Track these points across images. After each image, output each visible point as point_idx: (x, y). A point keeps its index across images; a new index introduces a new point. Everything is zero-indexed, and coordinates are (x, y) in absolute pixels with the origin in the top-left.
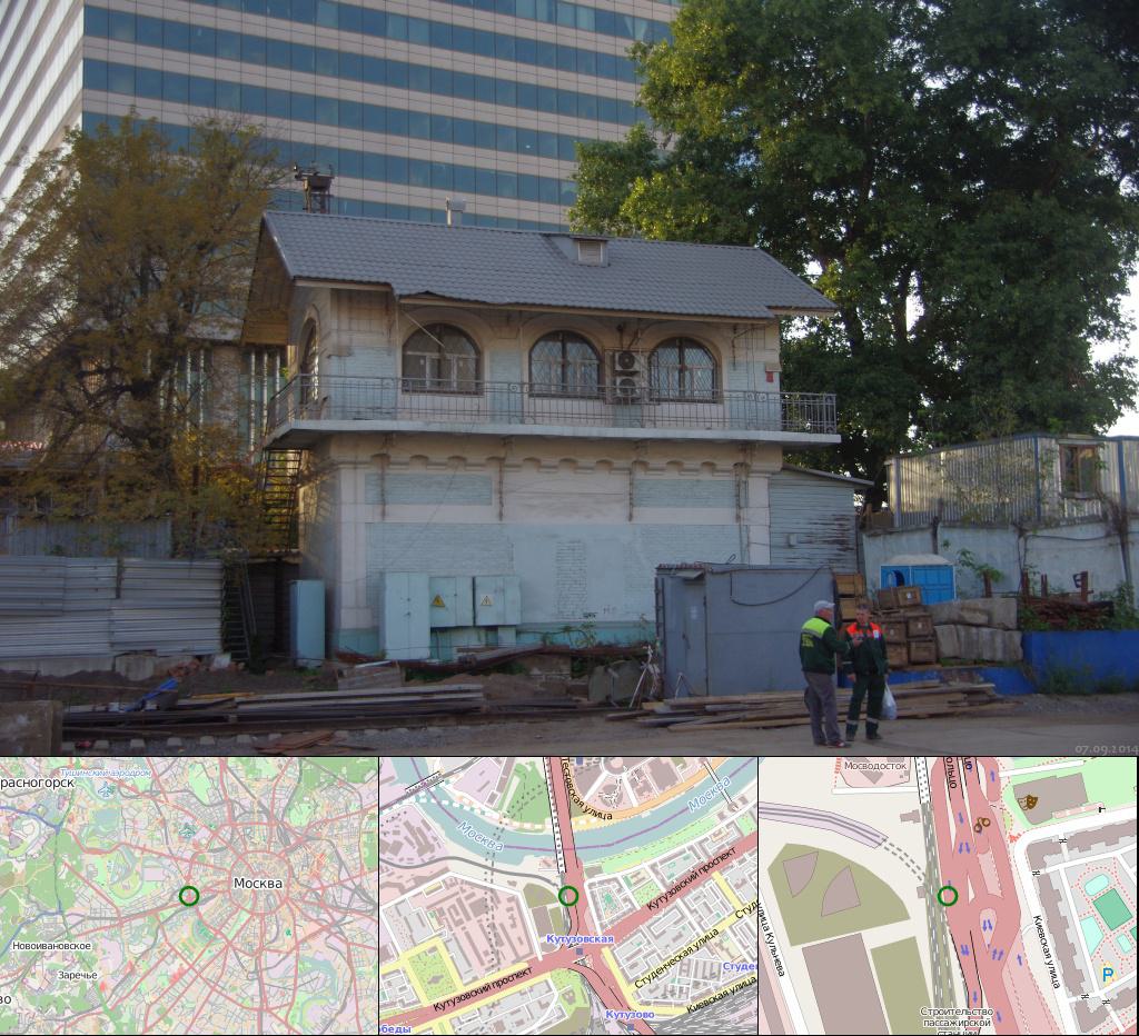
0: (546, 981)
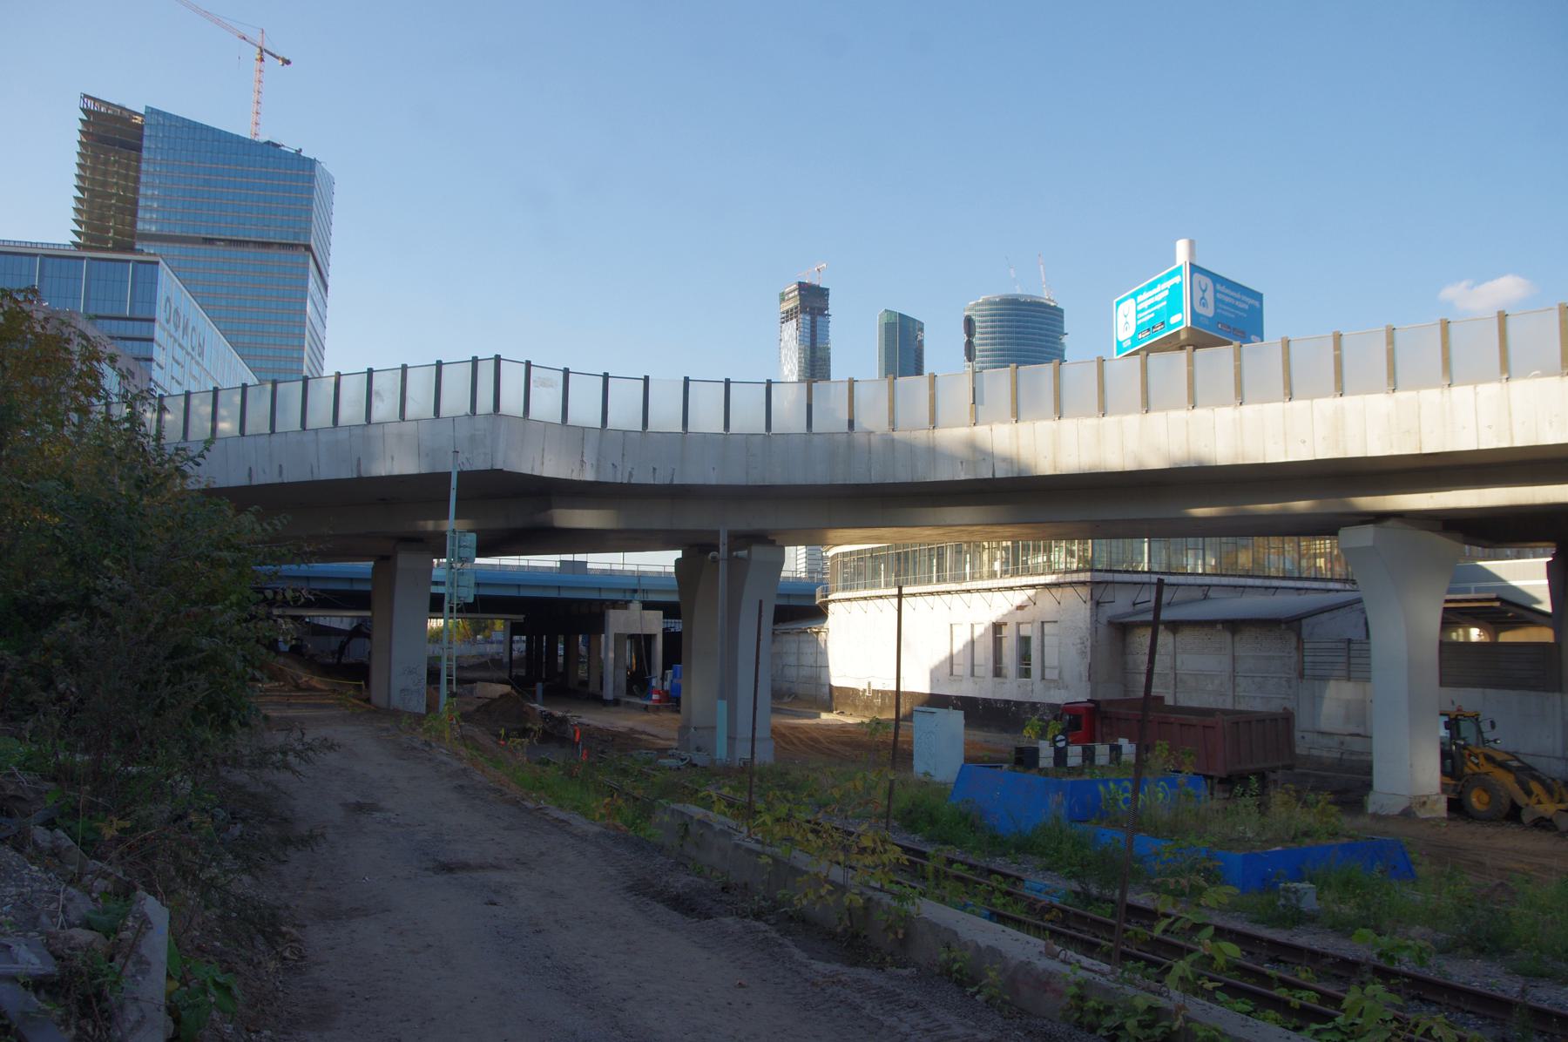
0: (1149, 601)
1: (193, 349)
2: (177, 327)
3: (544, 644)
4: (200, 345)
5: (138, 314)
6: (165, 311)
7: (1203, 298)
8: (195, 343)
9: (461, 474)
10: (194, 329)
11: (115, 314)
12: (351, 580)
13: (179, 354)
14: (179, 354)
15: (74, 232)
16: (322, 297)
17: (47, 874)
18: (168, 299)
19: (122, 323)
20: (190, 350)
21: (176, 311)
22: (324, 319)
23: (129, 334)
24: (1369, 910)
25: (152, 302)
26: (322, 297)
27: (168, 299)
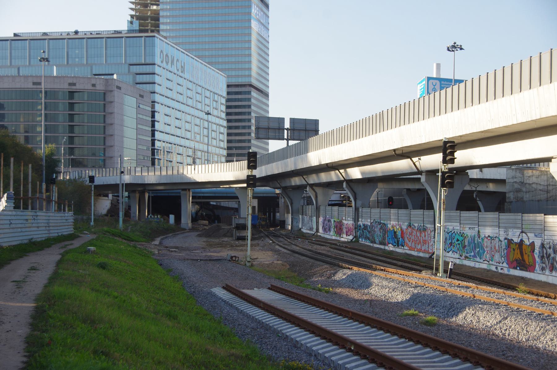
1: (178, 70)
2: (167, 63)
3: (272, 219)
4: (182, 67)
5: (148, 61)
6: (161, 58)
7: (434, 88)
8: (179, 67)
9: (293, 121)
10: (178, 60)
11: (138, 62)
12: (215, 193)
13: (170, 76)
14: (170, 76)
15: (132, 9)
16: (264, 13)
17: (506, 229)
18: (162, 52)
19: (141, 66)
20: (176, 71)
21: (167, 55)
22: (266, 25)
23: (144, 71)
24: (194, 354)
25: (153, 55)
26: (264, 13)
27: (162, 52)
